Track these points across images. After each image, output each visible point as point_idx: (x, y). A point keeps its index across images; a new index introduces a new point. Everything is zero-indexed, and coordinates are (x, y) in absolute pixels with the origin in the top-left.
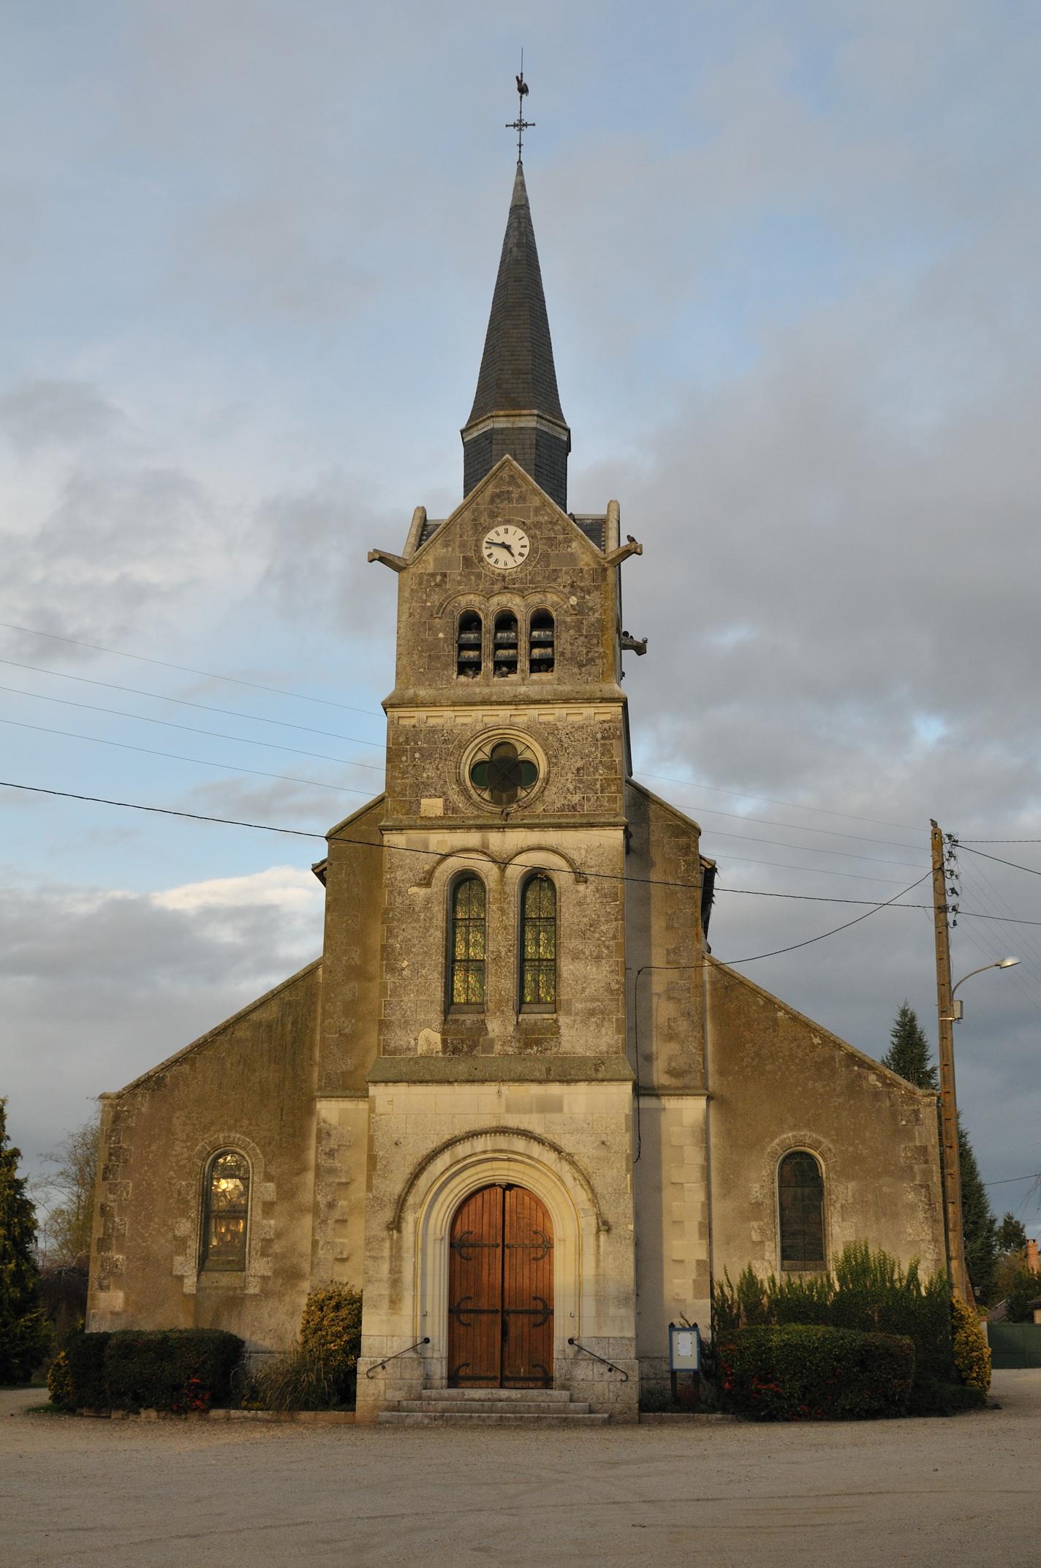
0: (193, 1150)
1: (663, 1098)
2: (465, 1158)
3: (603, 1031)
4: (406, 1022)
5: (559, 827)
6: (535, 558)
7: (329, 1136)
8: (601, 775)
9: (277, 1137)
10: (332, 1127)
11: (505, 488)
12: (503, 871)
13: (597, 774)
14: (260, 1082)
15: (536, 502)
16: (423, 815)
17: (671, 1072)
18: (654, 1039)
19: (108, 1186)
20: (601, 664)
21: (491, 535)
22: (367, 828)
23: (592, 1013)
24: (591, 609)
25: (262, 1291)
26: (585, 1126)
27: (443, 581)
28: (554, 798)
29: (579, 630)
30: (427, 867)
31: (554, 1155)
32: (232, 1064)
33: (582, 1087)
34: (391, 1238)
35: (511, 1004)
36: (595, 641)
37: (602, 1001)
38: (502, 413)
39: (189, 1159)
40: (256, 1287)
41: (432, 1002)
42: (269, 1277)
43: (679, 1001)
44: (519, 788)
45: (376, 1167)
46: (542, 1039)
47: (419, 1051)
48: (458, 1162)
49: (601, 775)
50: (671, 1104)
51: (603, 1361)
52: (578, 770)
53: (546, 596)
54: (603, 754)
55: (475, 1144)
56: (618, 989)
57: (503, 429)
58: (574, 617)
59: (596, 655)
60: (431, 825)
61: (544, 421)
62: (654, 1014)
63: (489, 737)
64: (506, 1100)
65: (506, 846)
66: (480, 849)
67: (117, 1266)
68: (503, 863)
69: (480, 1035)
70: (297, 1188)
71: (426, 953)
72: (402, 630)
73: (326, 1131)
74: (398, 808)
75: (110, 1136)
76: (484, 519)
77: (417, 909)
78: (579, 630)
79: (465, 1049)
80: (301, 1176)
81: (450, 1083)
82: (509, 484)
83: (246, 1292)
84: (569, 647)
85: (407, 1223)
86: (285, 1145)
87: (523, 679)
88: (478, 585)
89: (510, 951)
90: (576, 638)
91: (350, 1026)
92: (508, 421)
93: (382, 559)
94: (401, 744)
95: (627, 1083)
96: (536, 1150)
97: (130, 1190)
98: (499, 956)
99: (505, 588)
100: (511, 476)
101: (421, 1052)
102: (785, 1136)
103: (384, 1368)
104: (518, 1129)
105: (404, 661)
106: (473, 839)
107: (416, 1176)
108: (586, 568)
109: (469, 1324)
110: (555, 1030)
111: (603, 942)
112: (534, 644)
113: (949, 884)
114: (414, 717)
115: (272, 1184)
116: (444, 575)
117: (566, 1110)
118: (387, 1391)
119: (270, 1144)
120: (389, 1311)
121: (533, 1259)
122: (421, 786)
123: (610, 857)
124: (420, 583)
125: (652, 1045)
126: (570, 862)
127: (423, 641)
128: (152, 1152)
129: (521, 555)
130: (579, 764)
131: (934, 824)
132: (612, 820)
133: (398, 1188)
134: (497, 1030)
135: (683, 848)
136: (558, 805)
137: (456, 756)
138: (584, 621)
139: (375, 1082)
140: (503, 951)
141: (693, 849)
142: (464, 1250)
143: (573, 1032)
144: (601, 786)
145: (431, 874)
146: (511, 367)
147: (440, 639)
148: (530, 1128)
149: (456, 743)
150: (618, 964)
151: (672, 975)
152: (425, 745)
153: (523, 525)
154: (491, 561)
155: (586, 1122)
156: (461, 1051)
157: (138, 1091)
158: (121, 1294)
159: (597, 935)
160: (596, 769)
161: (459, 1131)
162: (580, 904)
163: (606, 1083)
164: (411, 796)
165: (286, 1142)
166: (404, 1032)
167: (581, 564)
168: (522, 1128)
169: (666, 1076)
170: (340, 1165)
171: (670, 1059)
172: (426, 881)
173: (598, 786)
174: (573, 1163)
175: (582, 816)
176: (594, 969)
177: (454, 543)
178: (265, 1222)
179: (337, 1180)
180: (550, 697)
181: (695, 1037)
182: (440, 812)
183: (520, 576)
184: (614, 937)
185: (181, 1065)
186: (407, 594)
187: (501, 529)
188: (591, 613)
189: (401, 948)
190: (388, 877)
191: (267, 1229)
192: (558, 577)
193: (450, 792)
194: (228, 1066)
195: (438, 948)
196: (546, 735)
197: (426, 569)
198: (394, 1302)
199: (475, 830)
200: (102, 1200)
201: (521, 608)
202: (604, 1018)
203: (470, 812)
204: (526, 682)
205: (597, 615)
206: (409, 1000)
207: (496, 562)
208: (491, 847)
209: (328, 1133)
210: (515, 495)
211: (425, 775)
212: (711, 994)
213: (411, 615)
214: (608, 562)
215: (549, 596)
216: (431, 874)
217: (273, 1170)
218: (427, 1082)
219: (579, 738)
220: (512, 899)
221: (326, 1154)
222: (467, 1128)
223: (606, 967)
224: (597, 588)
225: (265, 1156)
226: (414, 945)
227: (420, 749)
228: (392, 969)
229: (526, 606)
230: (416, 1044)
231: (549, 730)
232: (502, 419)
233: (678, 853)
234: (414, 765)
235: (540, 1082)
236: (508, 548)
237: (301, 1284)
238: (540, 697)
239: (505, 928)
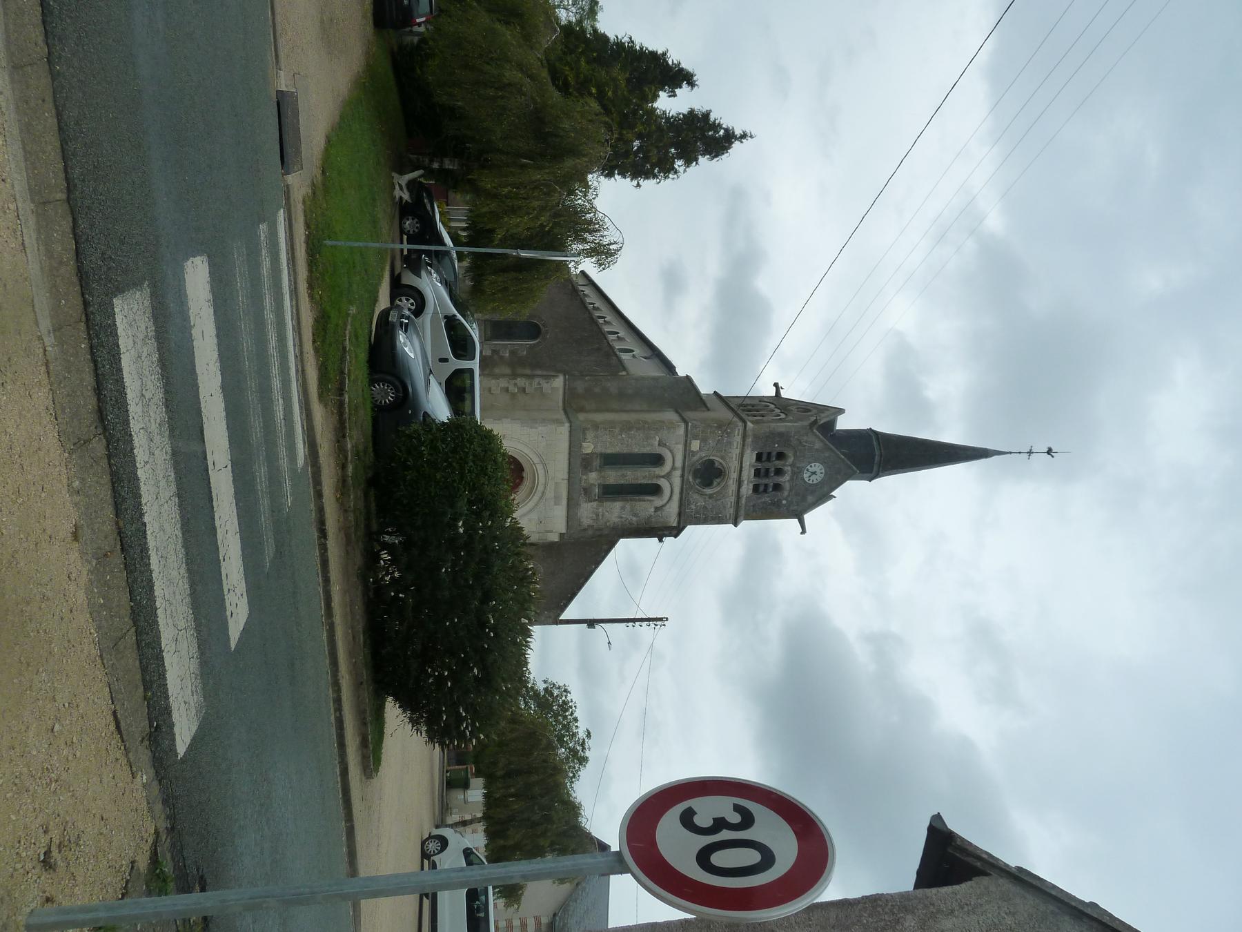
23: (597, 515)
44: (685, 82)
60: (686, 445)
98: (626, 476)
106: (679, 464)
112: (766, 486)
117: (555, 507)
145: (665, 445)
160: (705, 515)
201: (785, 479)
223: (617, 520)
239: (637, 479)
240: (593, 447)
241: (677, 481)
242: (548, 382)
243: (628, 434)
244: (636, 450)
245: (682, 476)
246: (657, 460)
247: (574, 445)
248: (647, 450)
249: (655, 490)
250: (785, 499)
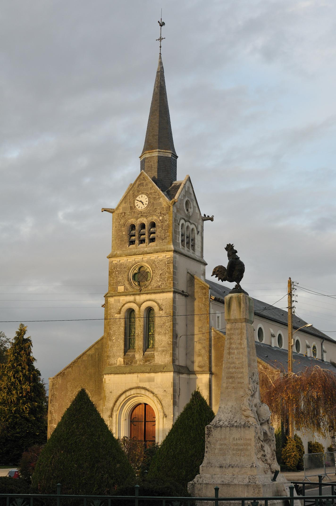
0: (73, 394)
1: (197, 375)
2: (129, 396)
3: (166, 356)
4: (114, 356)
5: (155, 293)
6: (150, 205)
8: (167, 275)
9: (94, 389)
11: (142, 182)
13: (166, 275)
14: (90, 373)
15: (150, 185)
17: (200, 367)
18: (195, 356)
19: (51, 405)
20: (168, 239)
21: (138, 198)
24: (166, 220)
26: (160, 386)
27: (125, 215)
28: (154, 284)
29: (162, 228)
31: (152, 395)
32: (82, 368)
33: (160, 374)
35: (142, 349)
36: (167, 231)
38: (147, 152)
39: (72, 396)
43: (202, 344)
46: (150, 359)
47: (118, 364)
48: (127, 397)
49: (167, 275)
50: (199, 376)
52: (161, 274)
53: (153, 217)
54: (167, 269)
55: (131, 392)
56: (170, 344)
57: (148, 158)
58: (161, 224)
59: (167, 236)
61: (161, 153)
62: (195, 348)
63: (137, 265)
66: (133, 301)
68: (140, 306)
69: (133, 359)
71: (119, 334)
72: (113, 232)
75: (52, 390)
76: (136, 193)
78: (162, 228)
79: (130, 363)
81: (125, 374)
82: (143, 180)
84: (159, 234)
86: (96, 392)
87: (146, 246)
88: (134, 215)
89: (141, 333)
90: (161, 231)
92: (149, 154)
93: (105, 211)
94: (112, 270)
95: (171, 372)
96: (147, 393)
97: (57, 406)
99: (142, 216)
100: (144, 178)
105: (114, 242)
106: (131, 298)
107: (116, 402)
108: (164, 207)
110: (153, 356)
113: (293, 299)
114: (115, 260)
116: (125, 213)
117: (155, 381)
119: (93, 391)
122: (118, 283)
123: (169, 302)
124: (118, 216)
125: (194, 358)
126: (158, 304)
127: (119, 235)
128: (62, 395)
129: (146, 204)
130: (161, 273)
131: (290, 278)
132: (169, 290)
133: (111, 405)
134: (138, 357)
135: (204, 294)
136: (155, 286)
137: (127, 272)
138: (164, 225)
139: (105, 374)
140: (140, 332)
141: (207, 294)
142: (134, 423)
143: (158, 357)
144: (167, 279)
145: (121, 310)
146: (152, 134)
147: (123, 234)
148: (146, 387)
149: (127, 268)
151: (200, 336)
152: (119, 269)
153: (147, 194)
154: (137, 207)
155: (160, 384)
156: (128, 364)
157: (58, 377)
159: (165, 327)
160: (166, 273)
163: (166, 373)
164: (115, 286)
165: (97, 391)
167: (163, 206)
169: (198, 368)
171: (199, 362)
172: (119, 313)
173: (166, 279)
174: (157, 397)
175: (161, 289)
177: (128, 202)
180: (152, 252)
181: (207, 355)
182: (123, 290)
183: (146, 211)
184: (170, 327)
185: (69, 369)
186: (115, 220)
187: (140, 196)
188: (166, 222)
192: (156, 211)
193: (126, 284)
194: (81, 368)
196: (152, 263)
197: (120, 211)
199: (132, 296)
200: (50, 409)
202: (167, 353)
203: (131, 290)
204: (147, 246)
205: (167, 222)
206: (115, 349)
207: (139, 207)
208: (137, 300)
210: (145, 184)
211: (119, 279)
212: (214, 341)
213: (116, 227)
214: (170, 204)
215: (154, 217)
216: (121, 310)
218: (119, 374)
219: (161, 264)
222: (129, 387)
223: (167, 336)
224: (167, 213)
226: (116, 332)
227: (118, 271)
228: (110, 340)
229: (147, 221)
230: (117, 362)
231: (152, 262)
232: (148, 154)
233: (203, 295)
234: (116, 276)
235: (148, 373)
236: (142, 203)
238: (149, 252)
239: (140, 326)
240: (120, 358)
241: (144, 297)
243: (113, 335)
244: (122, 329)
247: (118, 371)
249: (150, 310)
250: (159, 218)
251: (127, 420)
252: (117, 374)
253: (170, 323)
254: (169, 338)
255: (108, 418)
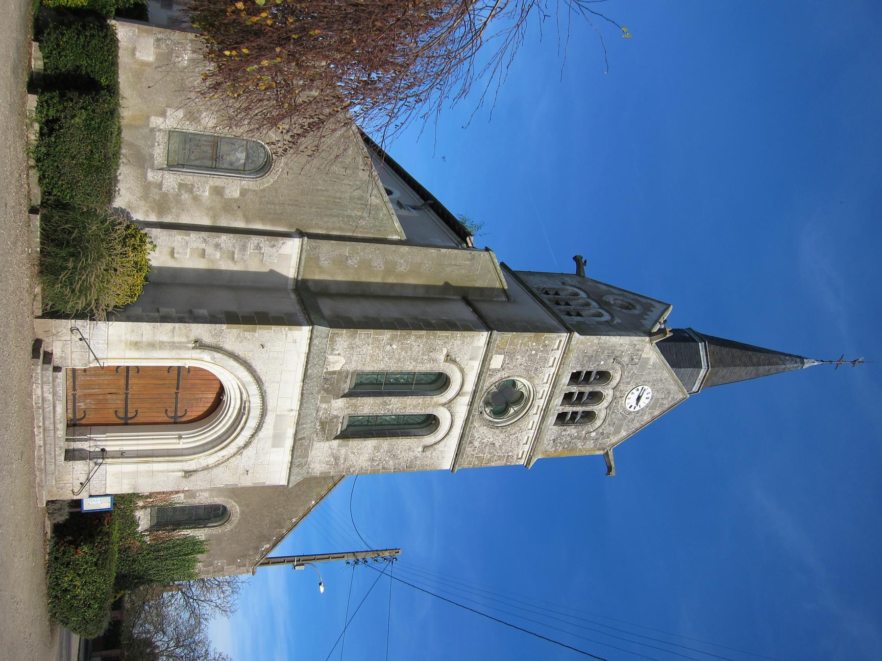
4: (353, 348)
7: (272, 246)
10: (278, 249)
12: (443, 405)
16: (493, 356)
22: (489, 277)
23: (337, 459)
25: (150, 183)
30: (458, 360)
33: (288, 458)
34: (188, 342)
35: (353, 412)
37: (343, 464)
40: (153, 177)
41: (364, 364)
42: (161, 189)
45: (246, 332)
47: (330, 357)
51: (88, 480)
60: (486, 360)
64: (286, 415)
65: (459, 406)
67: (178, 57)
70: (233, 214)
71: (400, 360)
73: (275, 244)
74: (503, 341)
77: (431, 354)
79: (326, 386)
80: (242, 218)
83: (149, 170)
85: (200, 353)
89: (389, 411)
91: (352, 264)
101: (329, 358)
102: (238, 508)
103: (81, 484)
104: (262, 426)
106: (469, 387)
109: (117, 372)
111: (382, 462)
115: (238, 195)
118: (61, 342)
120: (129, 342)
121: (166, 410)
123: (435, 463)
133: (228, 347)
143: (326, 449)
144: (480, 457)
145: (454, 361)
148: (263, 429)
150: (366, 471)
152: (538, 357)
158: (151, 59)
161: (269, 387)
162: (410, 449)
166: (346, 347)
168: (264, 425)
170: (248, 254)
172: (449, 358)
176: (365, 459)
178: (208, 188)
179: (236, 252)
184: (383, 468)
189: (407, 344)
190: (458, 335)
191: (201, 189)
195: (401, 367)
198: (136, 345)
201: (600, 409)
206: (368, 349)
209: (274, 246)
217: (250, 196)
220: (423, 411)
221: (258, 244)
225: (261, 190)
226: (406, 353)
227: (536, 354)
230: (336, 355)
237: (154, 214)
239: (405, 408)
242: (273, 246)
244: (410, 367)
245: (471, 404)
246: (440, 382)
248: (426, 367)
251: (179, 434)
252: (307, 362)
253: (393, 468)
254: (362, 468)
255: (193, 338)
